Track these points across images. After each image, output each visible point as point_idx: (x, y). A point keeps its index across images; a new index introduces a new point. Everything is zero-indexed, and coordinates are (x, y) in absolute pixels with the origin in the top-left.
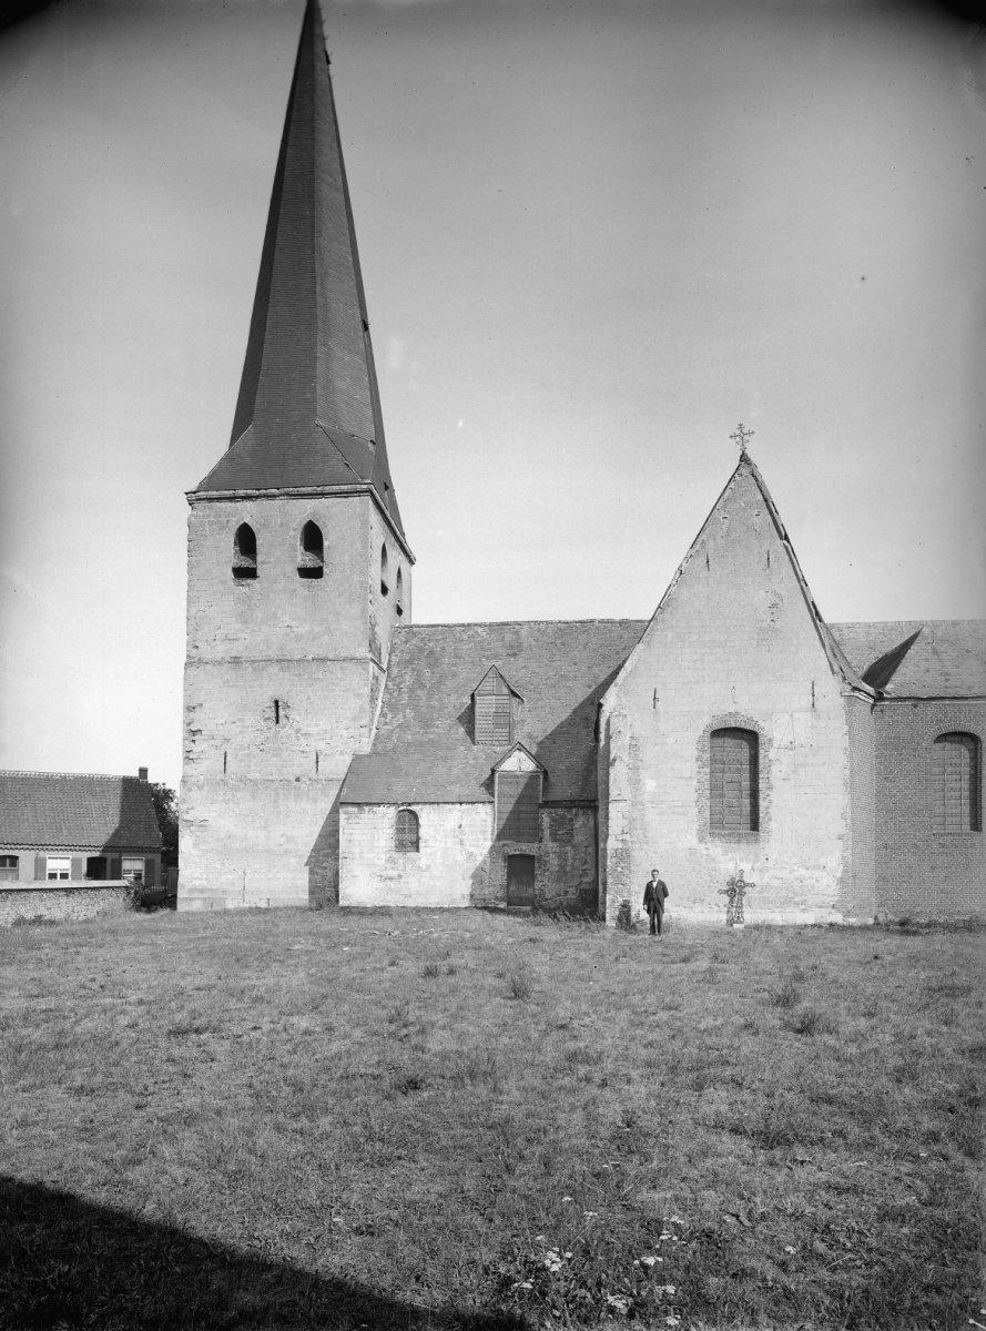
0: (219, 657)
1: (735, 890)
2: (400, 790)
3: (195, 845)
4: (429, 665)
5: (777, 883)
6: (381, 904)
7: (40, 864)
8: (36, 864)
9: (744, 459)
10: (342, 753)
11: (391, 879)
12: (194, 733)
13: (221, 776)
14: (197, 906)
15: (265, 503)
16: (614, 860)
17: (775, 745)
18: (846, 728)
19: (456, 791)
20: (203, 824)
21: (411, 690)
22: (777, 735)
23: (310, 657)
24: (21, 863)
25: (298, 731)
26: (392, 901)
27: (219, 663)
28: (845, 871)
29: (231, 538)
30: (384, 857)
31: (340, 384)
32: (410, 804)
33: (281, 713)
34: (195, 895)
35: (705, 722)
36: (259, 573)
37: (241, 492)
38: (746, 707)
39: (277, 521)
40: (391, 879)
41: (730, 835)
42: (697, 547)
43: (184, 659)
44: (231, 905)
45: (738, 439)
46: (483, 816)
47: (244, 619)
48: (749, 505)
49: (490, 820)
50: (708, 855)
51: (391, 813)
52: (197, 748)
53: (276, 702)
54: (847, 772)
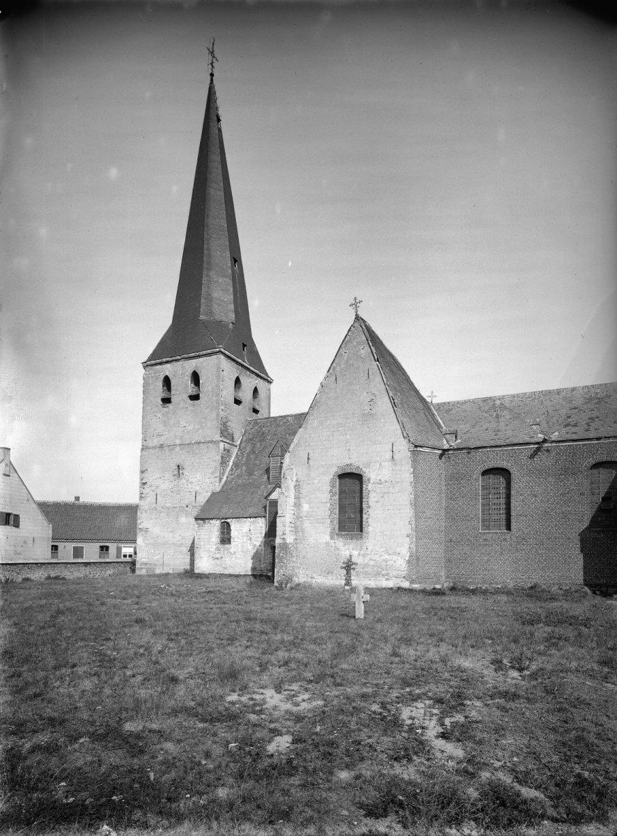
0: (154, 445)
1: (349, 566)
2: (225, 511)
3: (143, 541)
4: (260, 441)
5: (372, 563)
6: (213, 572)
7: (119, 549)
8: (510, 527)
9: (358, 318)
10: (207, 492)
11: (217, 559)
12: (144, 484)
13: (154, 505)
14: (144, 572)
15: (175, 363)
16: (279, 549)
17: (372, 482)
18: (412, 470)
19: (251, 511)
20: (147, 530)
21: (248, 455)
22: (371, 475)
23: (193, 442)
24: (59, 548)
25: (188, 481)
26: (218, 570)
27: (154, 448)
28: (411, 556)
29: (160, 384)
30: (214, 547)
31: (215, 295)
32: (226, 519)
33: (181, 472)
34: (143, 566)
35: (334, 470)
36: (172, 400)
37: (164, 360)
38: (355, 460)
39: (179, 371)
40: (217, 559)
41: (347, 535)
42: (331, 371)
43: (141, 447)
44: (158, 571)
45: (354, 306)
46: (261, 524)
47: (165, 423)
48: (359, 344)
49: (264, 526)
50: (335, 546)
51: (218, 523)
52: (145, 491)
53: (179, 466)
54: (412, 496)
